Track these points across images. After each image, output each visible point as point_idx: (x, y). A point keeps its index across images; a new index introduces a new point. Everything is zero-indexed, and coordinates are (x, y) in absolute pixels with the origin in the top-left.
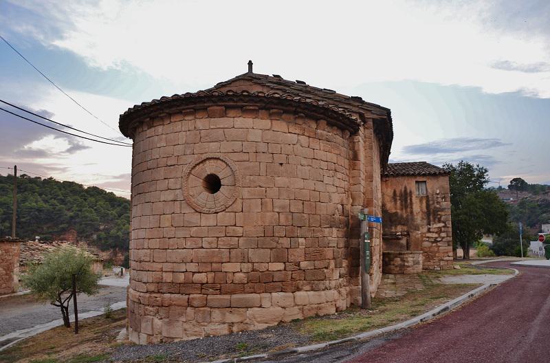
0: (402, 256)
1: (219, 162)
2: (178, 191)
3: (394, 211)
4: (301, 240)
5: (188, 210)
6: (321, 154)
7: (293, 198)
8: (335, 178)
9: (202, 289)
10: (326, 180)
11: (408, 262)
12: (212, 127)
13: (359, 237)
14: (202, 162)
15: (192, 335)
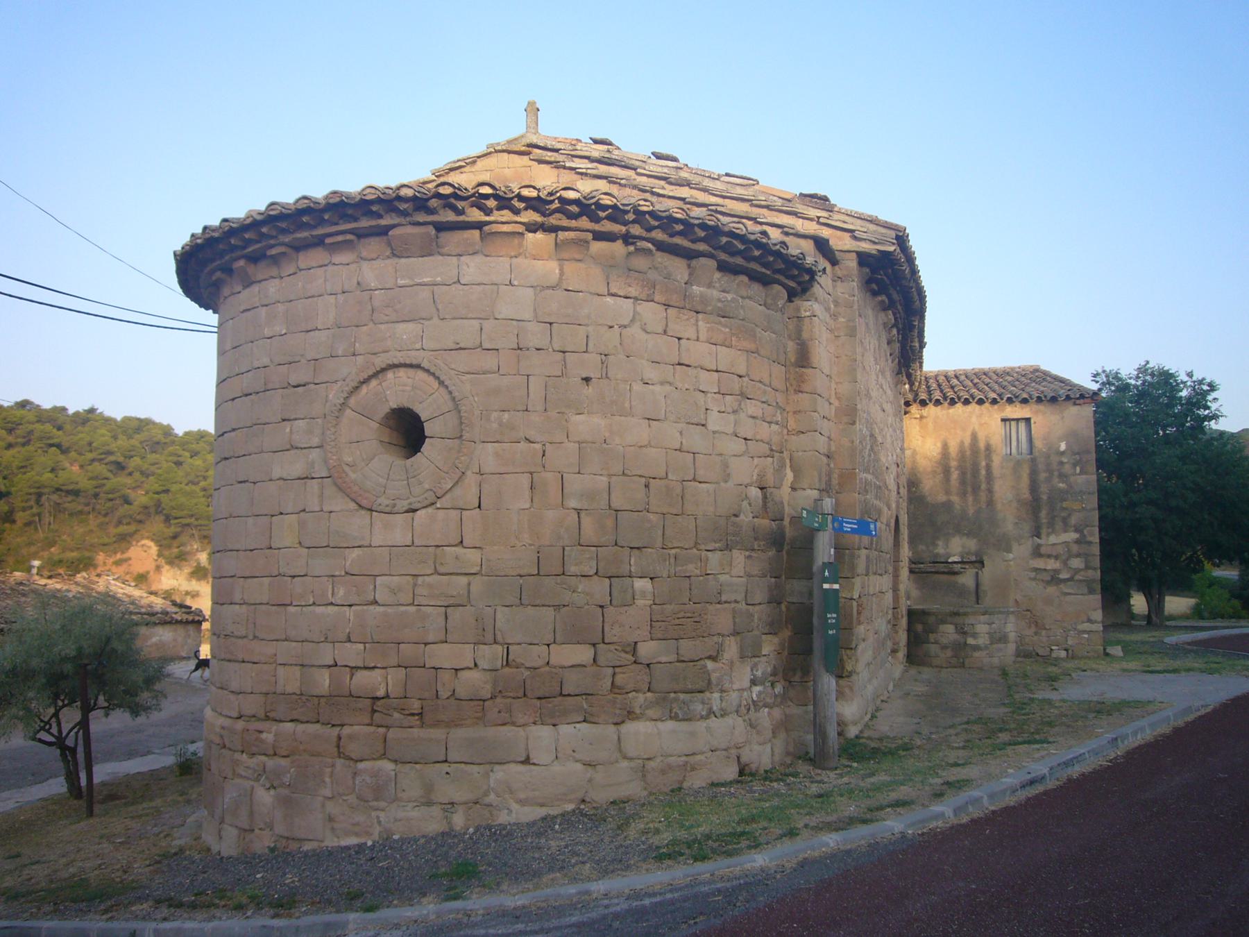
0: (959, 620)
1: (421, 375)
2: (315, 454)
3: (942, 498)
4: (641, 584)
5: (339, 504)
6: (699, 352)
7: (618, 468)
8: (742, 415)
9: (374, 711)
10: (714, 422)
11: (975, 635)
12: (401, 282)
13: (809, 576)
14: (375, 375)
15: (348, 834)
